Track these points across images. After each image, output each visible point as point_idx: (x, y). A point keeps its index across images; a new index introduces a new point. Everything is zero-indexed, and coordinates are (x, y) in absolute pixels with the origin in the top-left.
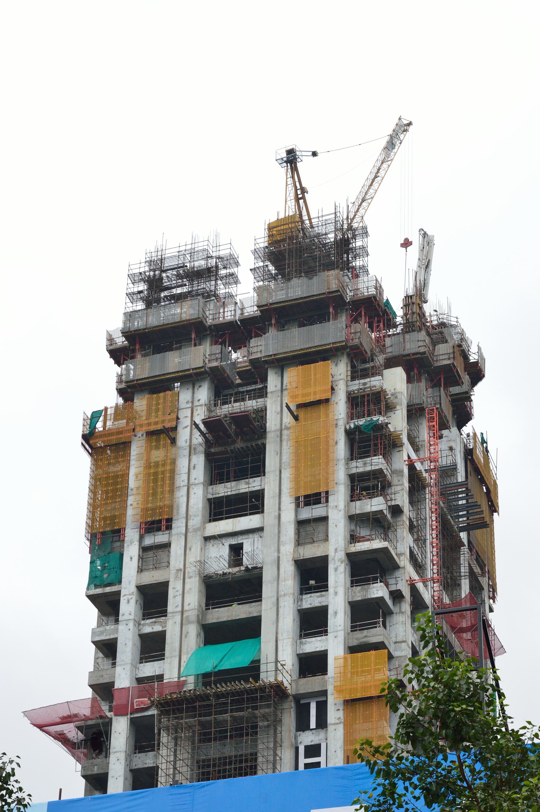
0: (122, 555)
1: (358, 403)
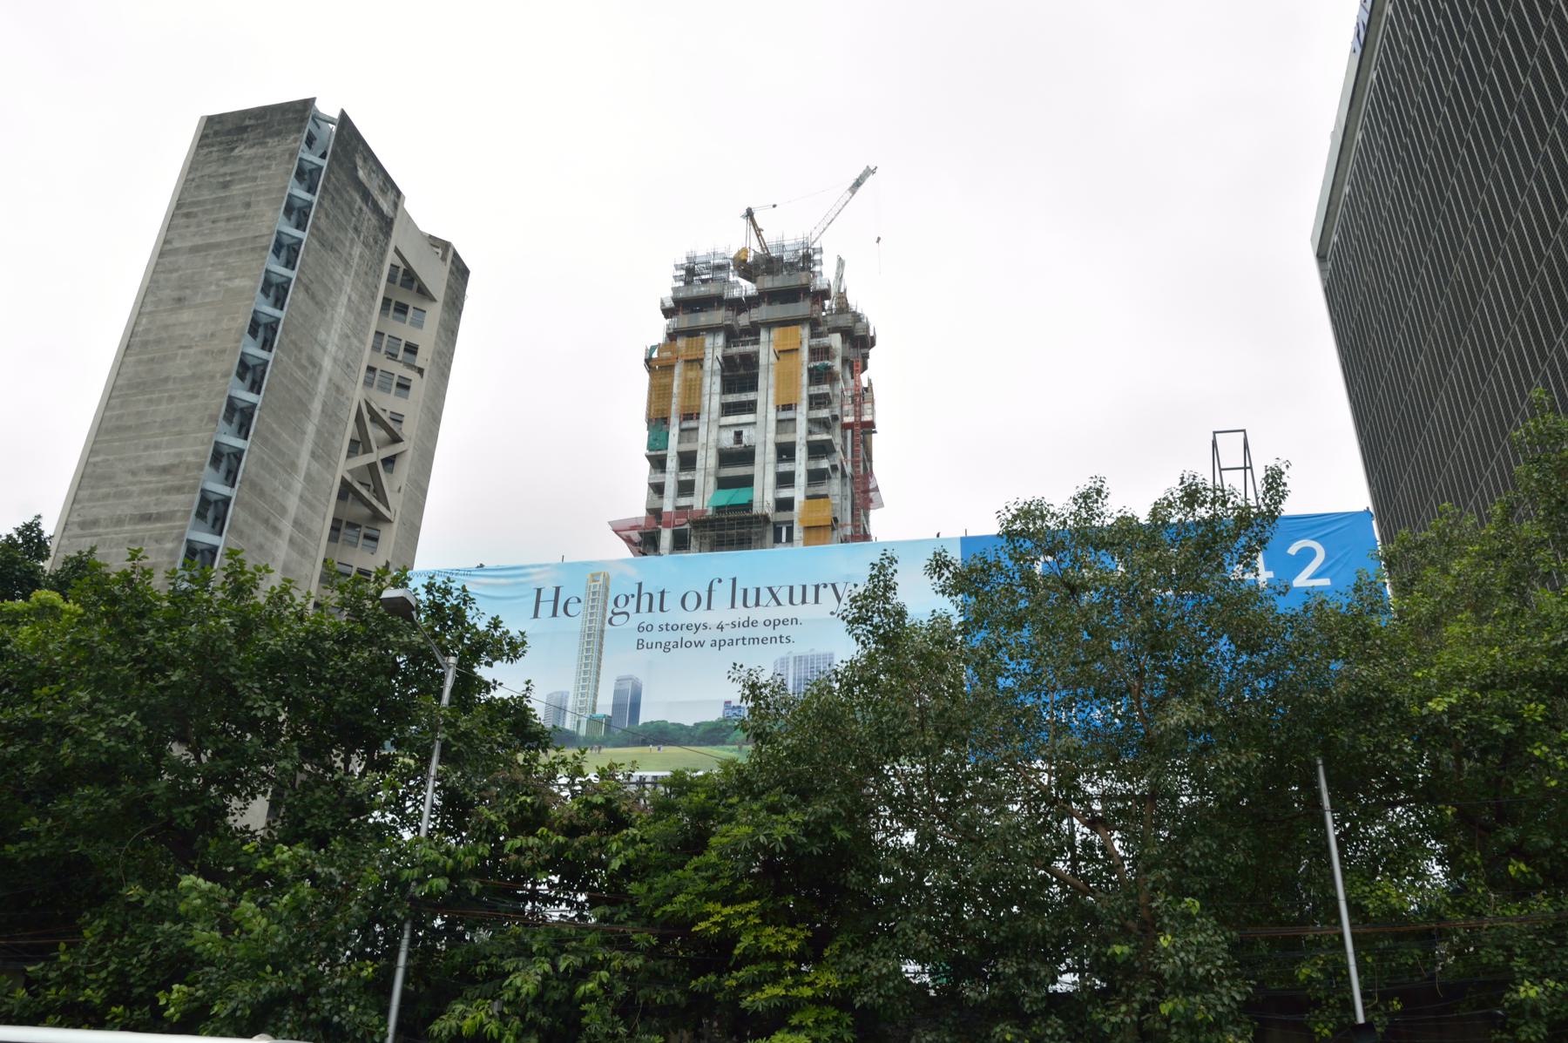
1: (815, 353)
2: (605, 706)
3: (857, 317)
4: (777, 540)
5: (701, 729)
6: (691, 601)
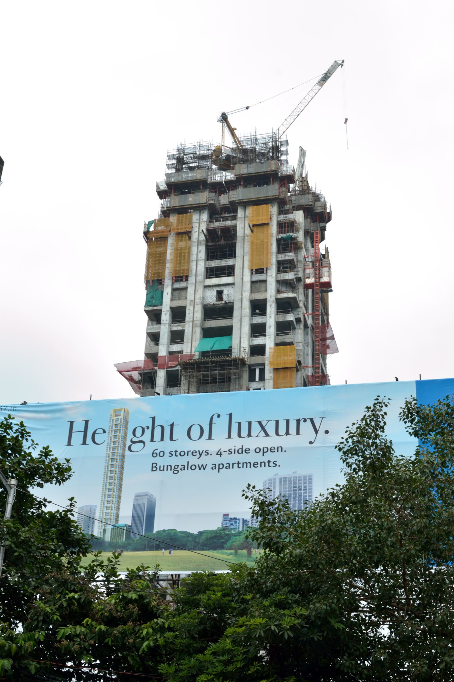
1: (282, 226)
2: (126, 517)
3: (317, 197)
4: (252, 379)
5: (204, 536)
6: (195, 432)
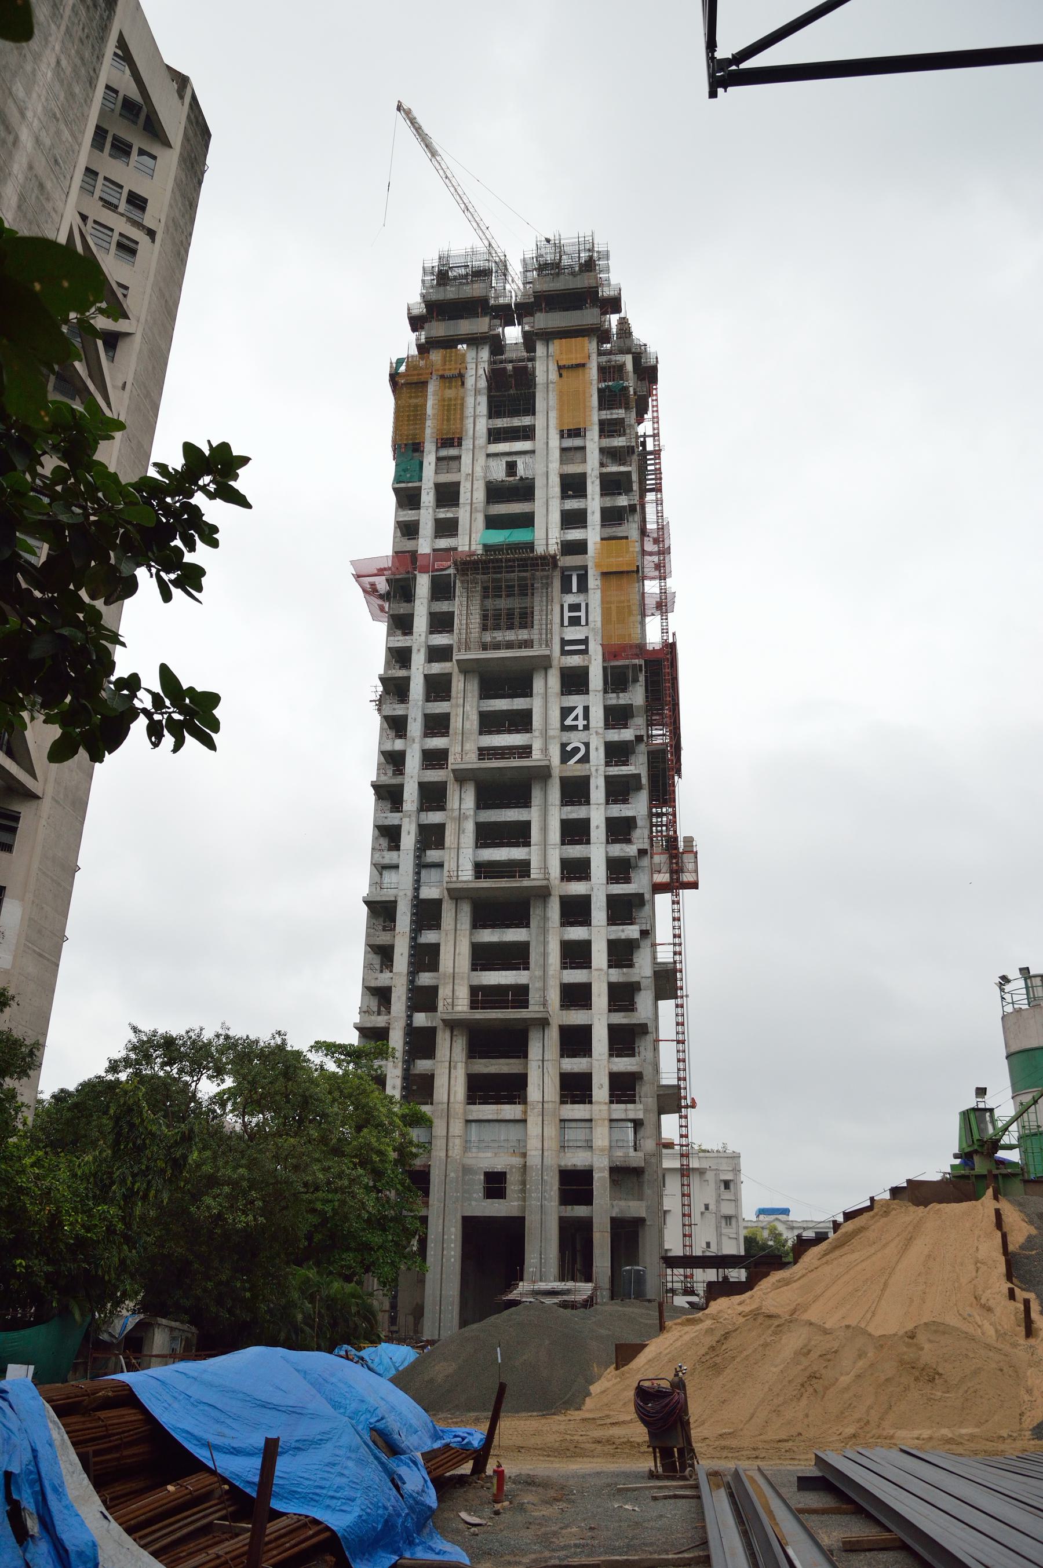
0: (421, 464)
1: (604, 371)
